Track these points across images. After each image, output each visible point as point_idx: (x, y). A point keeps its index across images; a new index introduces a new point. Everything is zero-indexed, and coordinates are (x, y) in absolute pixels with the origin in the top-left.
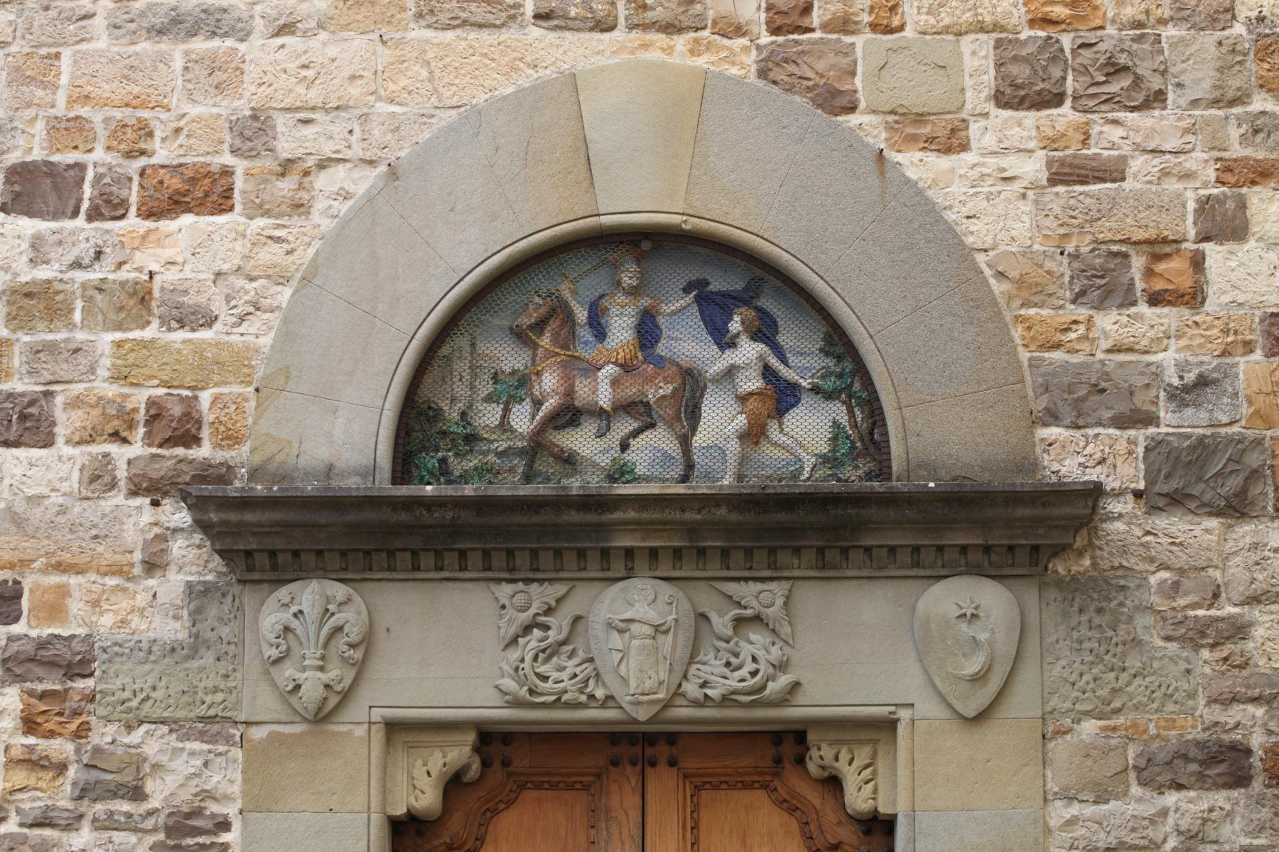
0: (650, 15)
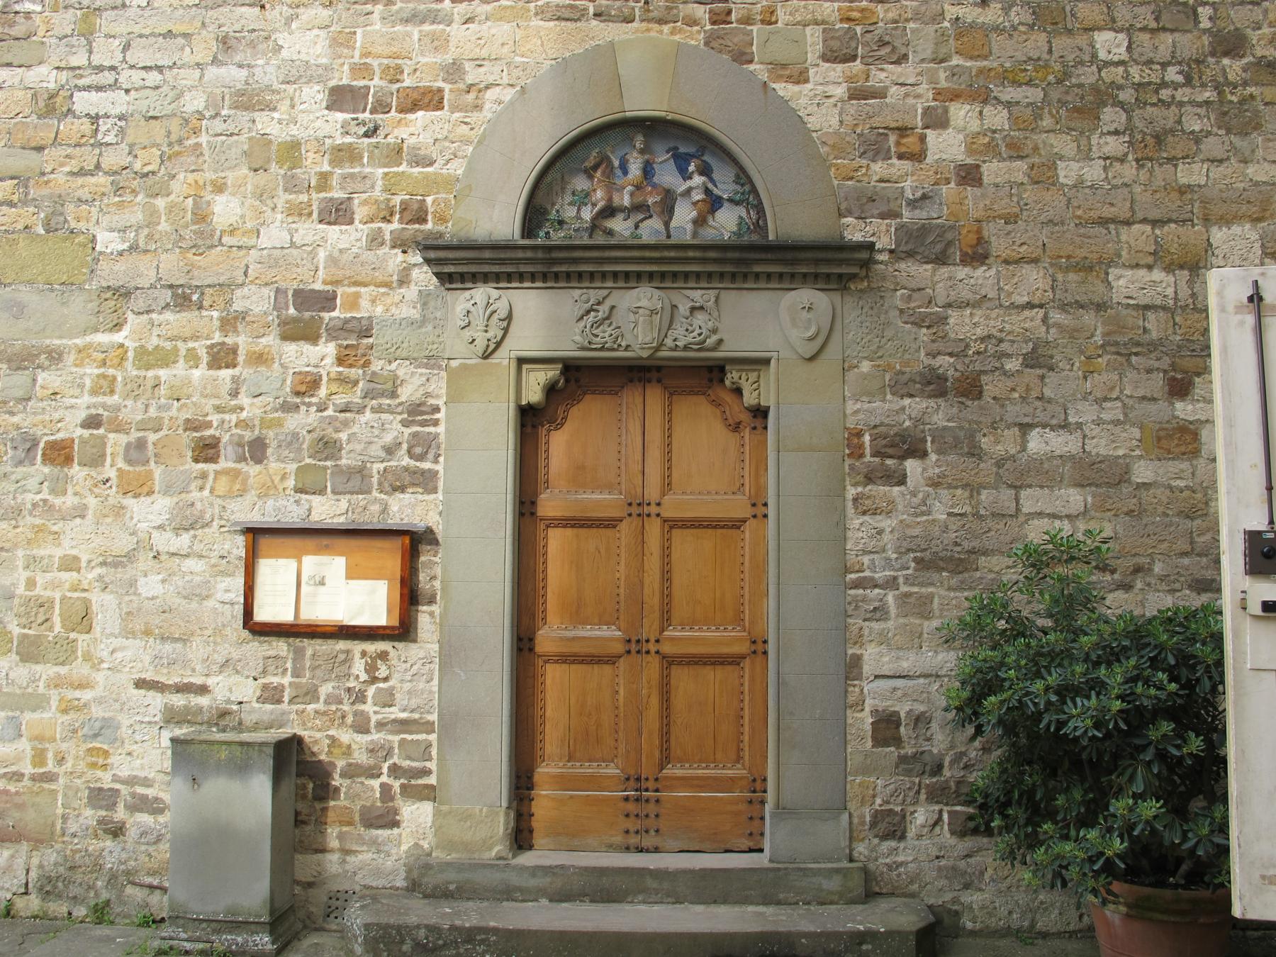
0: (651, 15)
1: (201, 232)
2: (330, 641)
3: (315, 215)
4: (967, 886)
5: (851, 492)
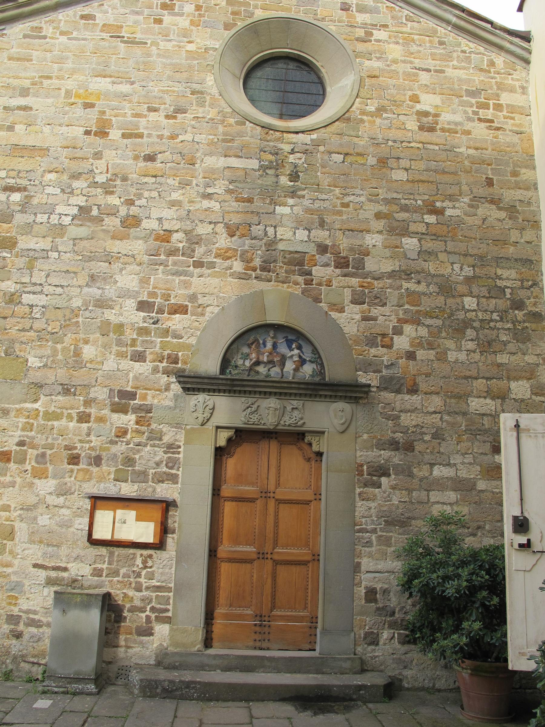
1: (77, 360)
2: (126, 549)
3: (129, 357)
4: (405, 667)
5: (358, 490)
